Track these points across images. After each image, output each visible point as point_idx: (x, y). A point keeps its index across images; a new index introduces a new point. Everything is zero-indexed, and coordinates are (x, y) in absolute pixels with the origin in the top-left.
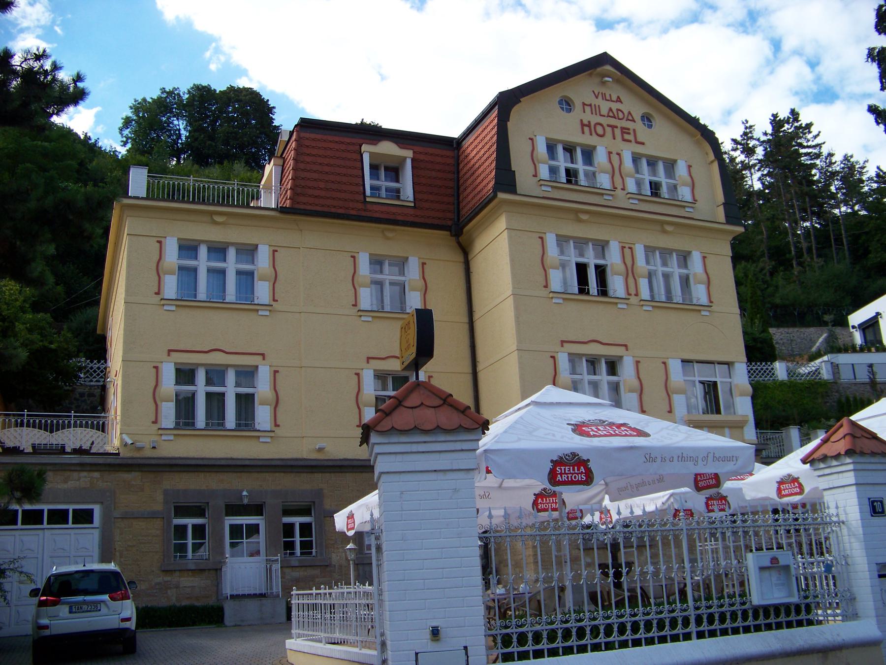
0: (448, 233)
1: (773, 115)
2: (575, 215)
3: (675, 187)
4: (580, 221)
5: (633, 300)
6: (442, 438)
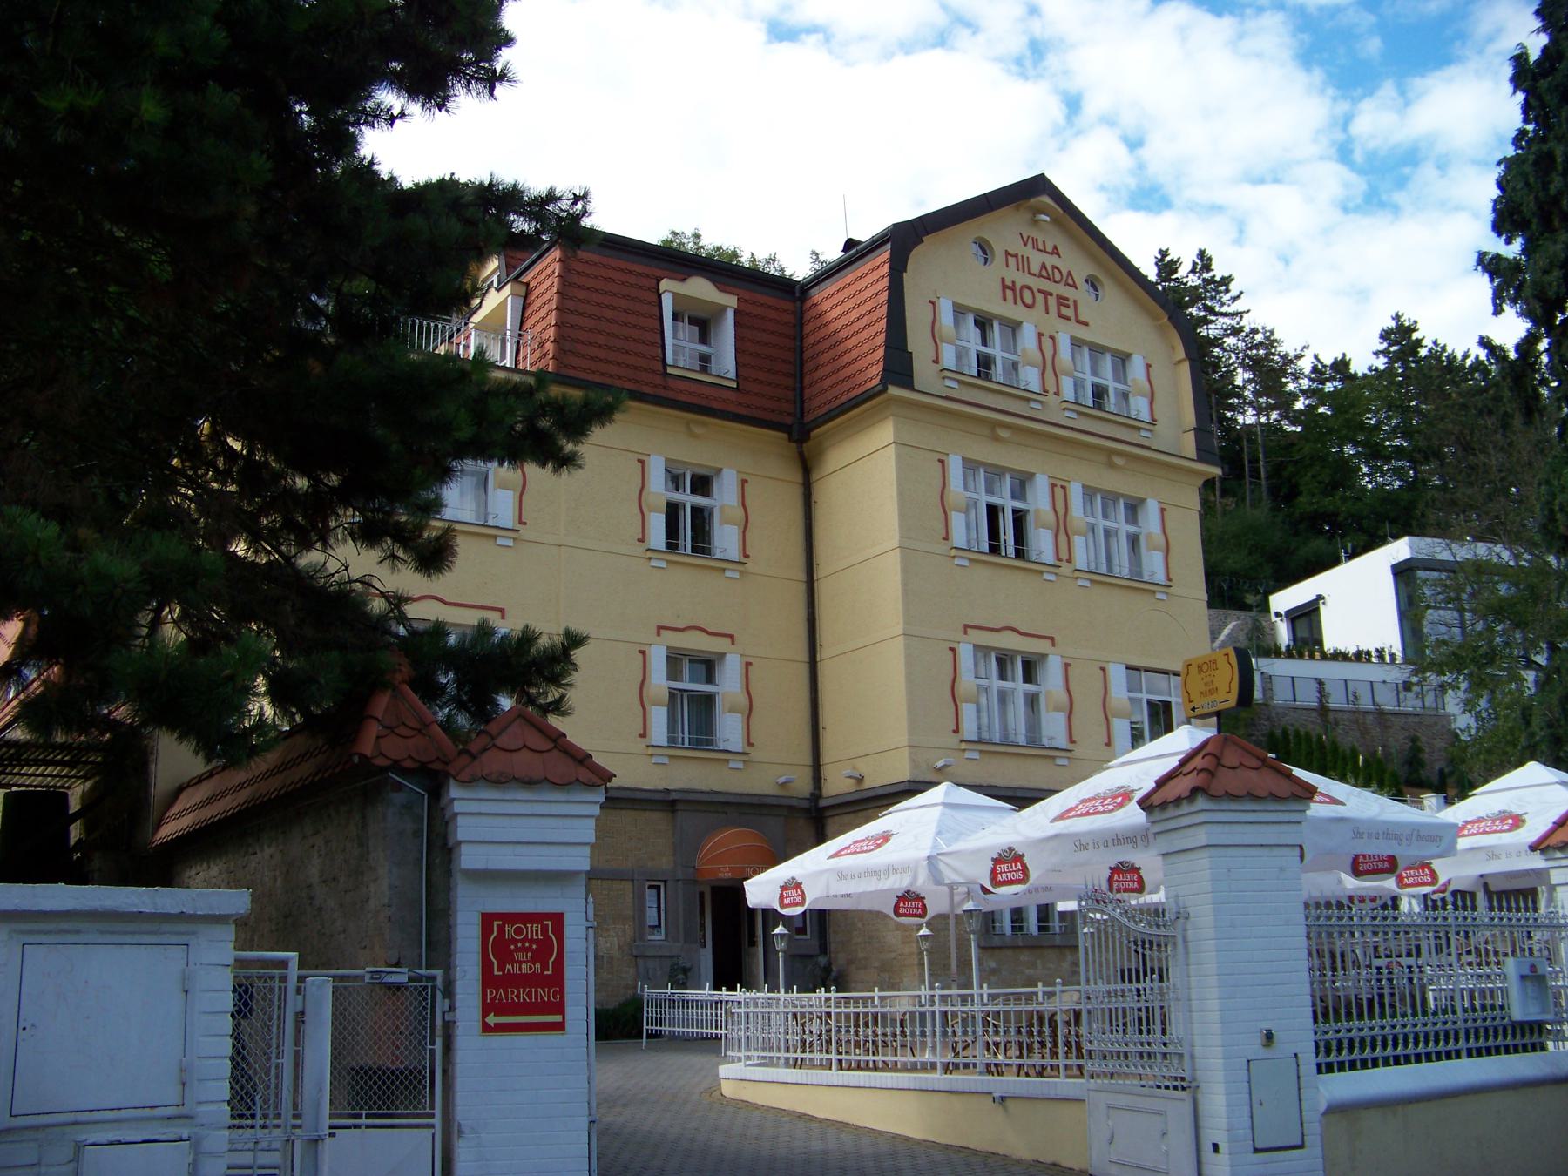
0: (785, 436)
1: (1160, 251)
2: (1109, 457)
3: (1125, 396)
4: (997, 439)
5: (1066, 569)
6: (1272, 806)
